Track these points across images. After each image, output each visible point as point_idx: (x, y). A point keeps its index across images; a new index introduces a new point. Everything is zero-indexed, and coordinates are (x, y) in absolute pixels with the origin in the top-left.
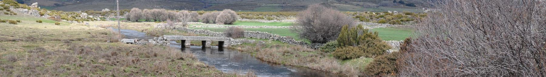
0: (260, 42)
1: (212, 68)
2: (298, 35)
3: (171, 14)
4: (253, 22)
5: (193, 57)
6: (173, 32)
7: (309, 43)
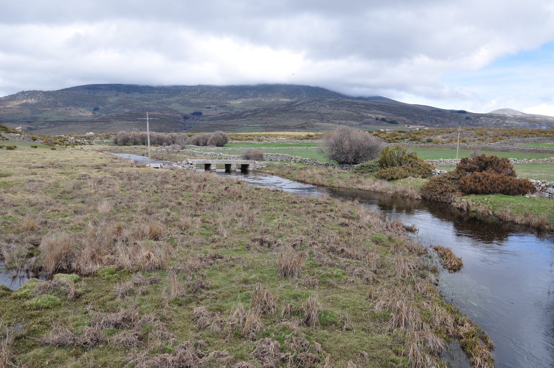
3: (160, 137)
4: (243, 144)
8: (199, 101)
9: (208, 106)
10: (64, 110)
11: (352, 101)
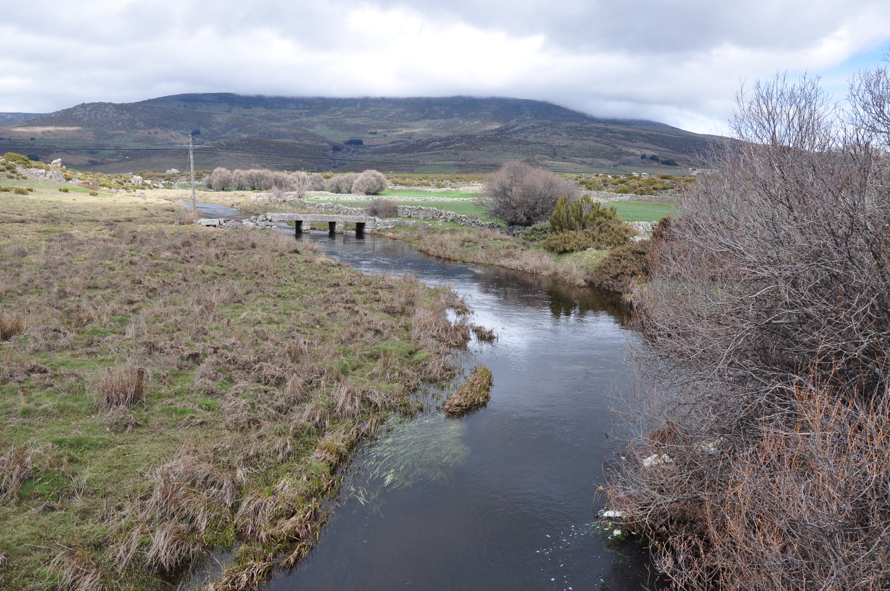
4: (412, 191)
8: (359, 122)
9: (373, 131)
10: (146, 134)
11: (605, 127)
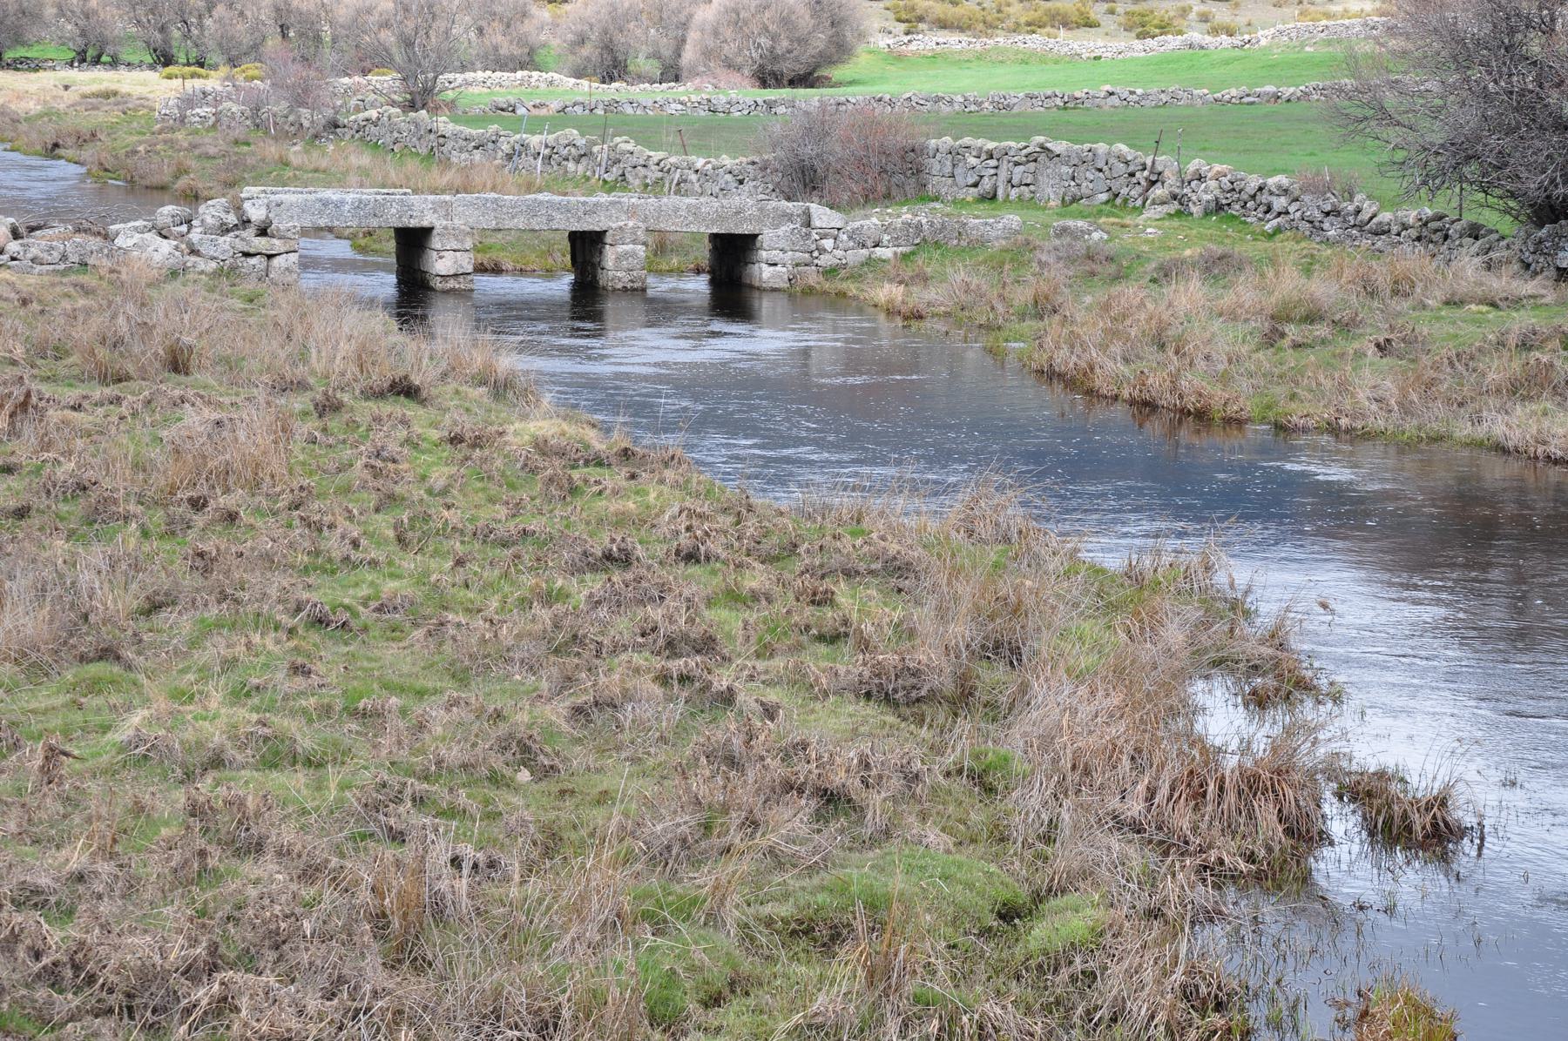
0: (1064, 230)
1: (666, 465)
2: (1400, 155)
5: (501, 376)
6: (324, 164)
7: (1506, 225)
